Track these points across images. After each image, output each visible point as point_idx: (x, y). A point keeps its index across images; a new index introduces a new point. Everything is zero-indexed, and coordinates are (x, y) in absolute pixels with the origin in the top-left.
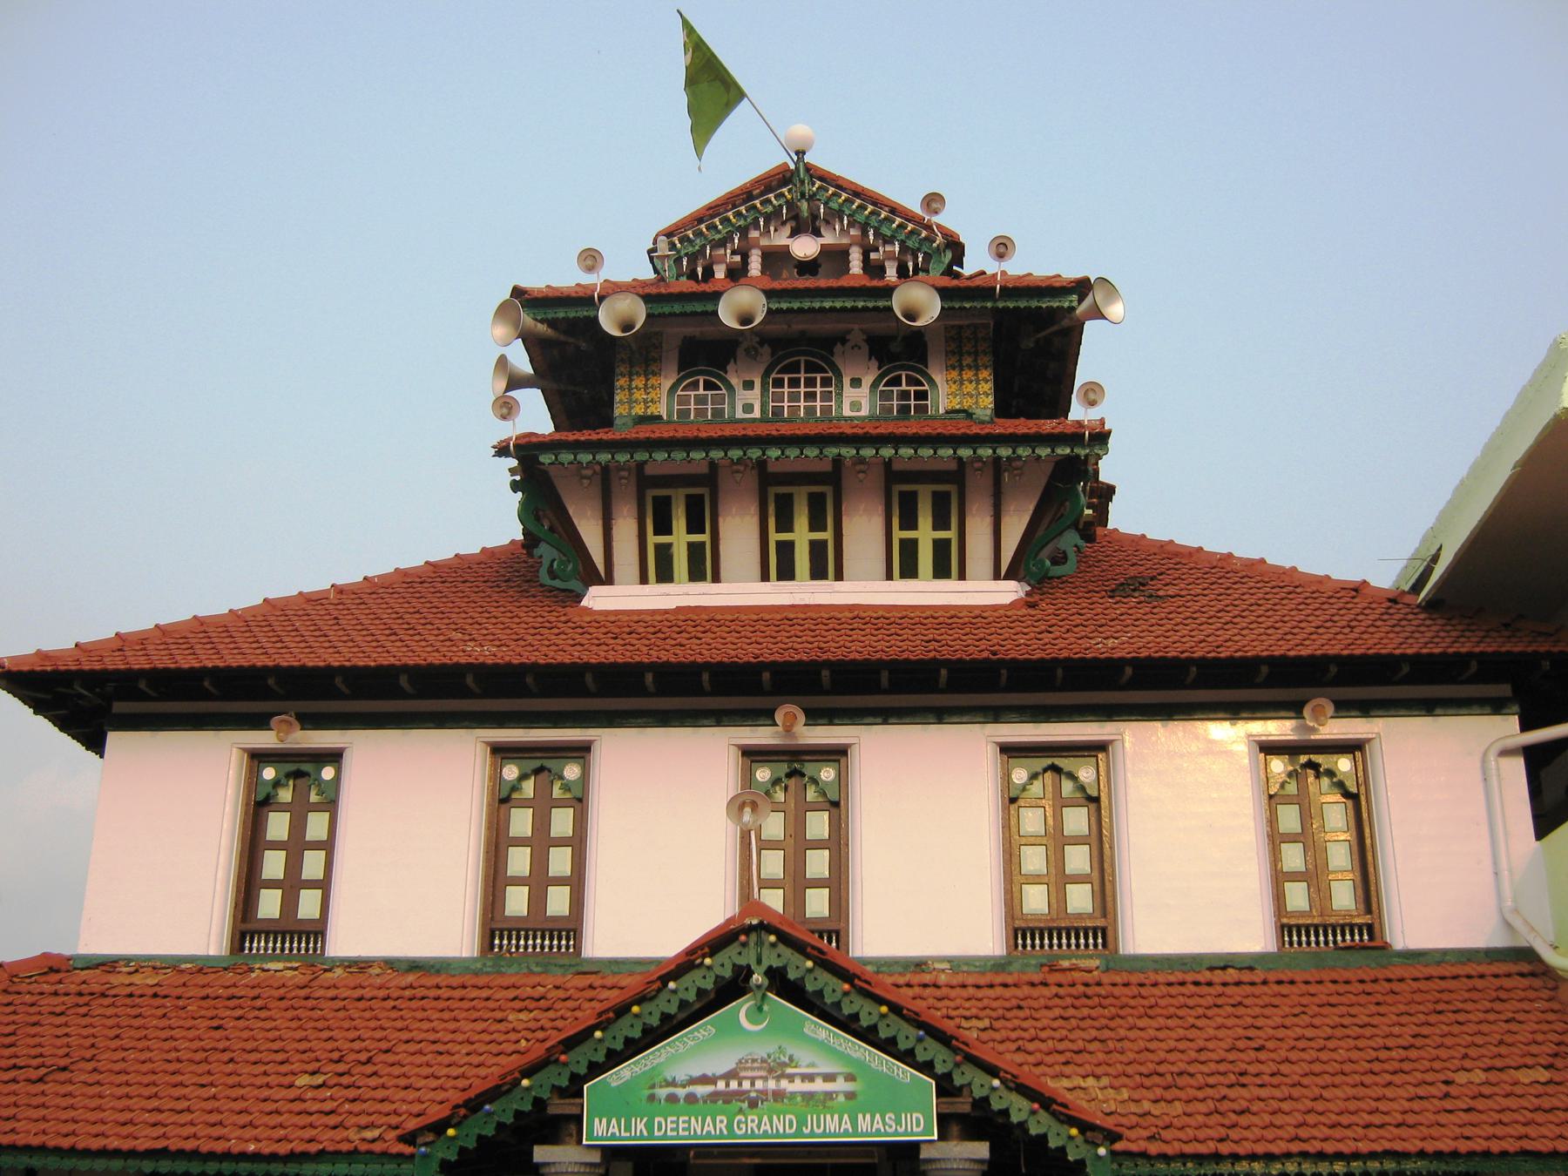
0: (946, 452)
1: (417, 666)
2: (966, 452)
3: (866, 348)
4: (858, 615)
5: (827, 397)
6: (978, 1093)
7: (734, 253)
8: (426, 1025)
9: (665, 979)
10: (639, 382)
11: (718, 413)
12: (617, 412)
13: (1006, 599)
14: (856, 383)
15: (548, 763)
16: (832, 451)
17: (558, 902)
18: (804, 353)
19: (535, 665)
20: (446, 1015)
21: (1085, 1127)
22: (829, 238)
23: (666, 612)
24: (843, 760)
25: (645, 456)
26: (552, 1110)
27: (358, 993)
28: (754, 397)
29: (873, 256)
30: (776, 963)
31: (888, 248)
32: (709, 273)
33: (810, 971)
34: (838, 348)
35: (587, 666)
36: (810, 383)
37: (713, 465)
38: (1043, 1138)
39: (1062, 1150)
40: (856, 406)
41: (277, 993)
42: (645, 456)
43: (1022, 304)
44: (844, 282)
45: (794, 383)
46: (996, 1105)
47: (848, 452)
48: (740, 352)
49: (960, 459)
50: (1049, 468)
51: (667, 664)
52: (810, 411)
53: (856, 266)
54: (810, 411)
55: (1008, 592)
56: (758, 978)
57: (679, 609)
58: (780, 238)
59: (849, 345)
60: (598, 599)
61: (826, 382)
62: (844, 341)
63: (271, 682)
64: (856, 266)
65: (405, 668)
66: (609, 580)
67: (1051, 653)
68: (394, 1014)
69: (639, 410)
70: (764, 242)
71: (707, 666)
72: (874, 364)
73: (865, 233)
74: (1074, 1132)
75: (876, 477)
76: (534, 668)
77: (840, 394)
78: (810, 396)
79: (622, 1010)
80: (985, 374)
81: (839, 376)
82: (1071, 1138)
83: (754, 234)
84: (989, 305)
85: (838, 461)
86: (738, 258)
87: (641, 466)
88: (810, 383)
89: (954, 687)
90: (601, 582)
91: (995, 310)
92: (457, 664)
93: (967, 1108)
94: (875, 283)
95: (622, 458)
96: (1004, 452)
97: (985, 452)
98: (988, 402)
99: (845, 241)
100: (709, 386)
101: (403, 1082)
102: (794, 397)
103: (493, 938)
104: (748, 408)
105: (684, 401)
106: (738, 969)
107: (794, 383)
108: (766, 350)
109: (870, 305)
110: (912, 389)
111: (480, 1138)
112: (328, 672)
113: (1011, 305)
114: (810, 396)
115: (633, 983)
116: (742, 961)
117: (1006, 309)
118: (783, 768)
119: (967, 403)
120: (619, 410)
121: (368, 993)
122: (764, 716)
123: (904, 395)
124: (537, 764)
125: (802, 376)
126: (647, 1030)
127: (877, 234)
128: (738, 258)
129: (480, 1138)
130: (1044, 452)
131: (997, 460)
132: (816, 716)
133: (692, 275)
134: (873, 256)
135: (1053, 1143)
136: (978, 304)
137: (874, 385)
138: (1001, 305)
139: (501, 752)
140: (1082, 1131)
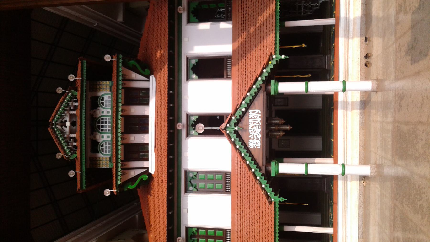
0: (120, 91)
1: (167, 210)
2: (120, 87)
3: (94, 110)
4: (157, 138)
5: (106, 119)
6: (261, 83)
7: (70, 141)
8: (246, 205)
9: (236, 149)
10: (101, 162)
11: (109, 144)
12: (109, 167)
13: (154, 79)
14: (103, 112)
15: (189, 180)
16: (120, 117)
17: (219, 177)
18: (95, 125)
19: (167, 183)
20: (244, 200)
21: (269, 60)
22: (67, 118)
23: (155, 155)
24: (189, 58)
25: (120, 160)
26: (264, 172)
27: (239, 220)
28: (105, 111)
29: (72, 108)
30: (233, 125)
31: (70, 104)
32: (75, 147)
33: (235, 118)
34: (94, 116)
35: (168, 171)
36: (102, 123)
37: (122, 144)
38: (271, 69)
39: (274, 65)
40: (108, 137)
41: (239, 239)
42: (120, 160)
43: (85, 73)
44: (78, 115)
45: (102, 126)
46: (264, 79)
47: (120, 113)
48: (94, 139)
49: (122, 88)
50: (124, 68)
51: (168, 153)
52: (109, 123)
53: (74, 112)
54: (109, 123)
55: (152, 78)
56: (236, 128)
57: (155, 152)
58: (67, 129)
59: (94, 114)
60: (152, 171)
61: (102, 119)
62: (92, 115)
63: (170, 228)
64: (74, 112)
65: (167, 212)
66: (148, 168)
67: (166, 81)
68: (244, 212)
69: (108, 162)
70: (68, 133)
71: (168, 144)
72: (98, 108)
73: (66, 110)
74: (270, 62)
75: (126, 107)
76: (168, 183)
77: (105, 116)
78: (106, 123)
79: (243, 158)
80: (101, 83)
81: (102, 116)
82: (271, 63)
83: (66, 136)
84: (85, 81)
85: (122, 116)
86: (72, 140)
87: (122, 161)
88: (102, 123)
89: (173, 50)
90: (148, 171)
91: (86, 80)
92: (167, 200)
93: (264, 85)
94: (79, 108)
95: (120, 165)
96: (121, 78)
97: (121, 82)
98: (108, 82)
99: (68, 115)
100: (102, 146)
101: (258, 208)
102: (106, 126)
103: (227, 191)
104: (108, 112)
105: (106, 152)
106: (234, 133)
107: (102, 126)
108: (94, 133)
109: (84, 108)
110: (104, 146)
111: (270, 187)
112: (168, 230)
113: (85, 76)
114: (106, 123)
115: (237, 155)
116: (233, 132)
117: (86, 77)
118: (191, 128)
119: (108, 87)
120: (108, 167)
121: (239, 218)
122: (179, 132)
123: (106, 148)
124: (189, 183)
125: (101, 125)
126: (247, 152)
127: (67, 107)
128: (72, 140)
129: (270, 187)
130: (121, 69)
131: (123, 80)
132: (179, 120)
133: (76, 151)
134: (72, 108)
135: (272, 67)
136: (85, 83)
137: (104, 108)
138: (85, 78)
139: (187, 191)
140: (270, 61)
